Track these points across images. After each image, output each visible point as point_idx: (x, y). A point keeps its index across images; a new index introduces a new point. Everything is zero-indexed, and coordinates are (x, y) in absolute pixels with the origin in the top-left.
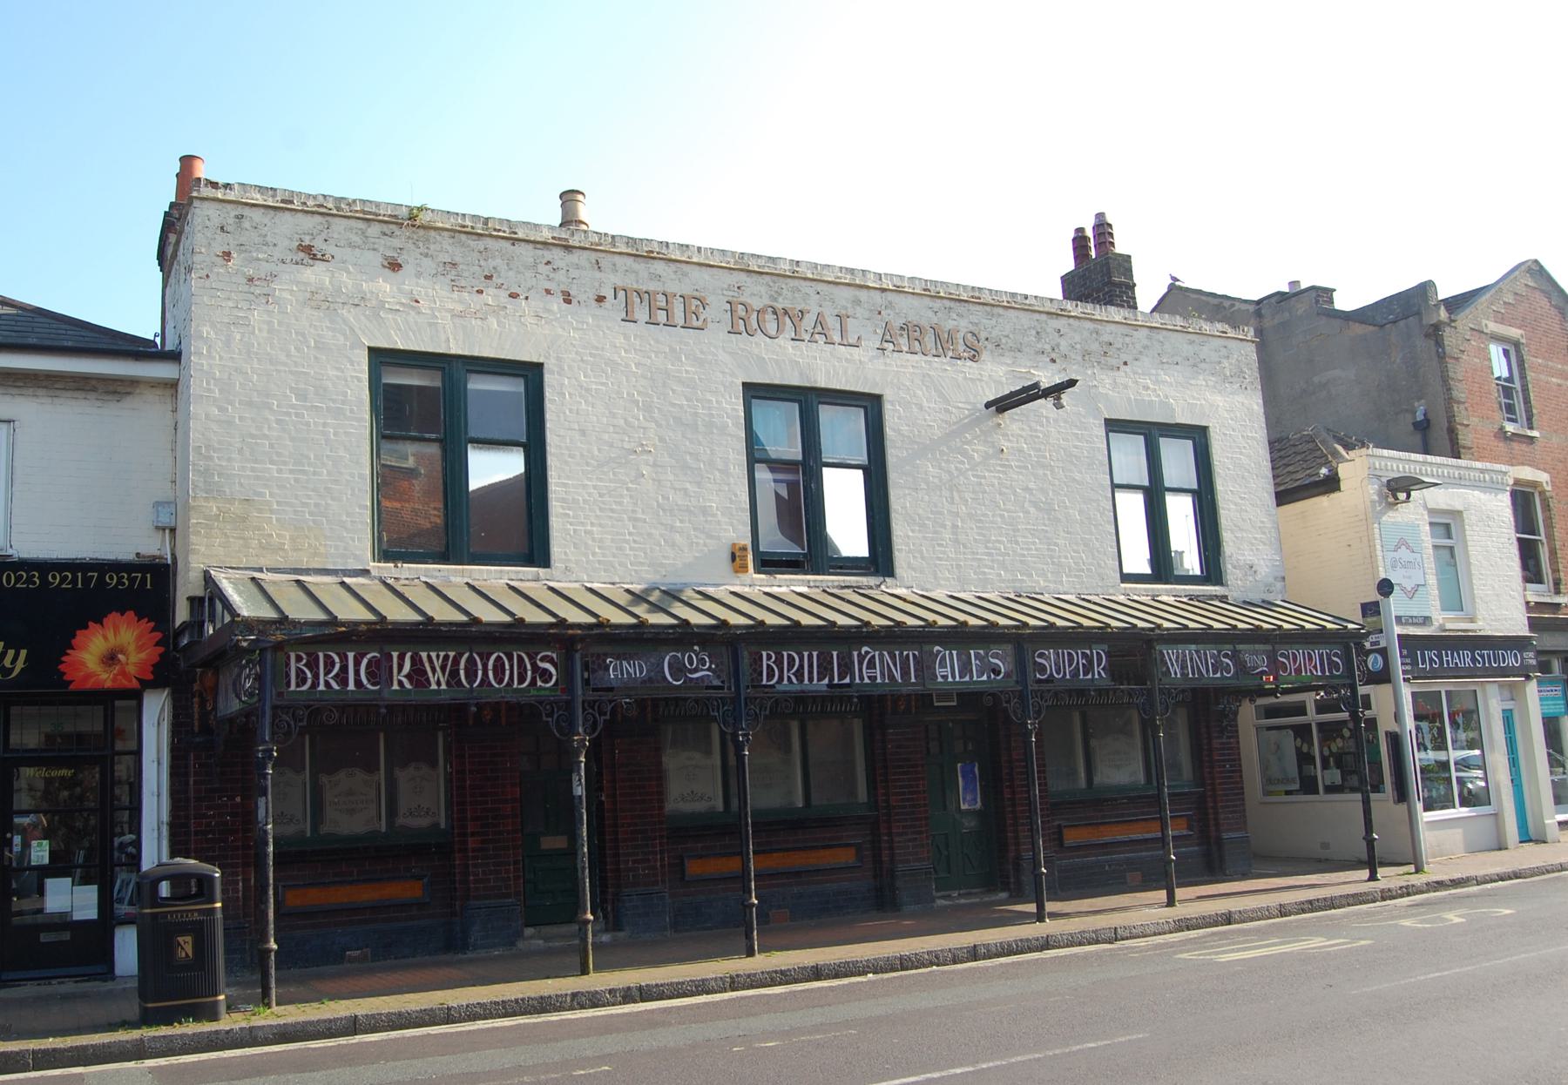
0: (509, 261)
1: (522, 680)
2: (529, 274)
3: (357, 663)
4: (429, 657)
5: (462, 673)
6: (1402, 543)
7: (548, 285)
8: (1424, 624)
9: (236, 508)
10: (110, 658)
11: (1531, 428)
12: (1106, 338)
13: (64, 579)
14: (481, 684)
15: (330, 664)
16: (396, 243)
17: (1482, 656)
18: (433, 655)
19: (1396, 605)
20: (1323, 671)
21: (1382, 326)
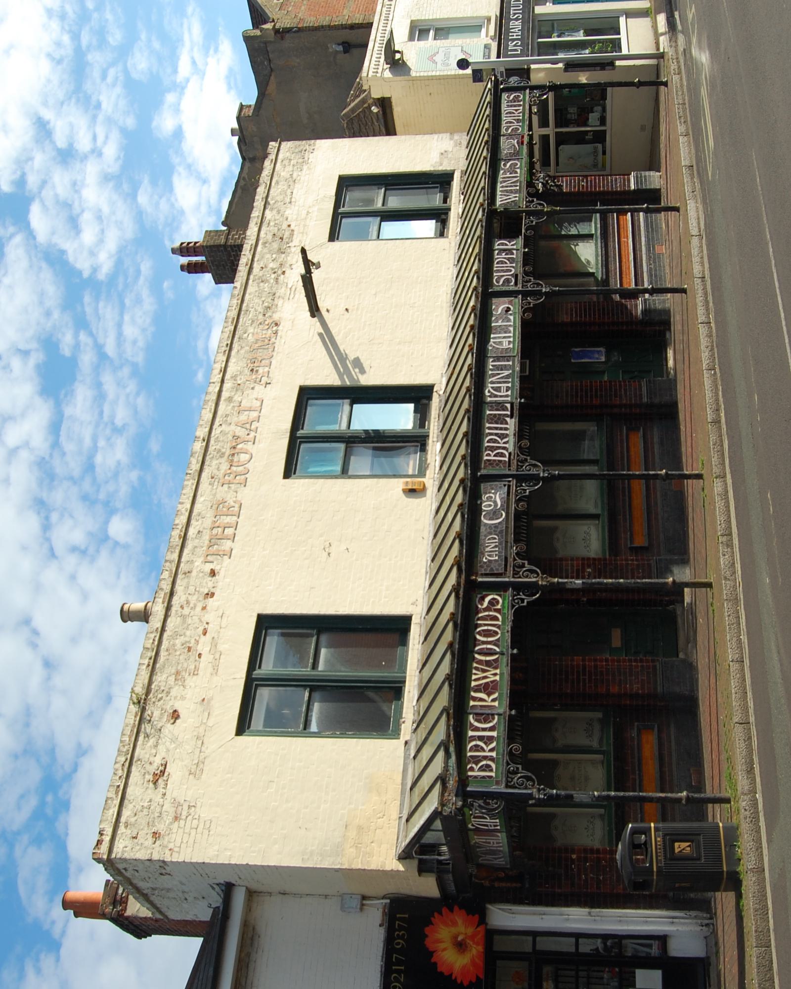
0: (176, 635)
1: (495, 618)
2: (189, 621)
3: (477, 729)
4: (475, 680)
5: (488, 658)
6: (431, 59)
7: (199, 609)
8: (490, 49)
9: (352, 834)
10: (461, 946)
12: (270, 237)
13: (397, 980)
15: (477, 748)
16: (157, 714)
17: (515, 14)
18: (474, 677)
19: (476, 57)
20: (520, 105)
21: (272, 70)
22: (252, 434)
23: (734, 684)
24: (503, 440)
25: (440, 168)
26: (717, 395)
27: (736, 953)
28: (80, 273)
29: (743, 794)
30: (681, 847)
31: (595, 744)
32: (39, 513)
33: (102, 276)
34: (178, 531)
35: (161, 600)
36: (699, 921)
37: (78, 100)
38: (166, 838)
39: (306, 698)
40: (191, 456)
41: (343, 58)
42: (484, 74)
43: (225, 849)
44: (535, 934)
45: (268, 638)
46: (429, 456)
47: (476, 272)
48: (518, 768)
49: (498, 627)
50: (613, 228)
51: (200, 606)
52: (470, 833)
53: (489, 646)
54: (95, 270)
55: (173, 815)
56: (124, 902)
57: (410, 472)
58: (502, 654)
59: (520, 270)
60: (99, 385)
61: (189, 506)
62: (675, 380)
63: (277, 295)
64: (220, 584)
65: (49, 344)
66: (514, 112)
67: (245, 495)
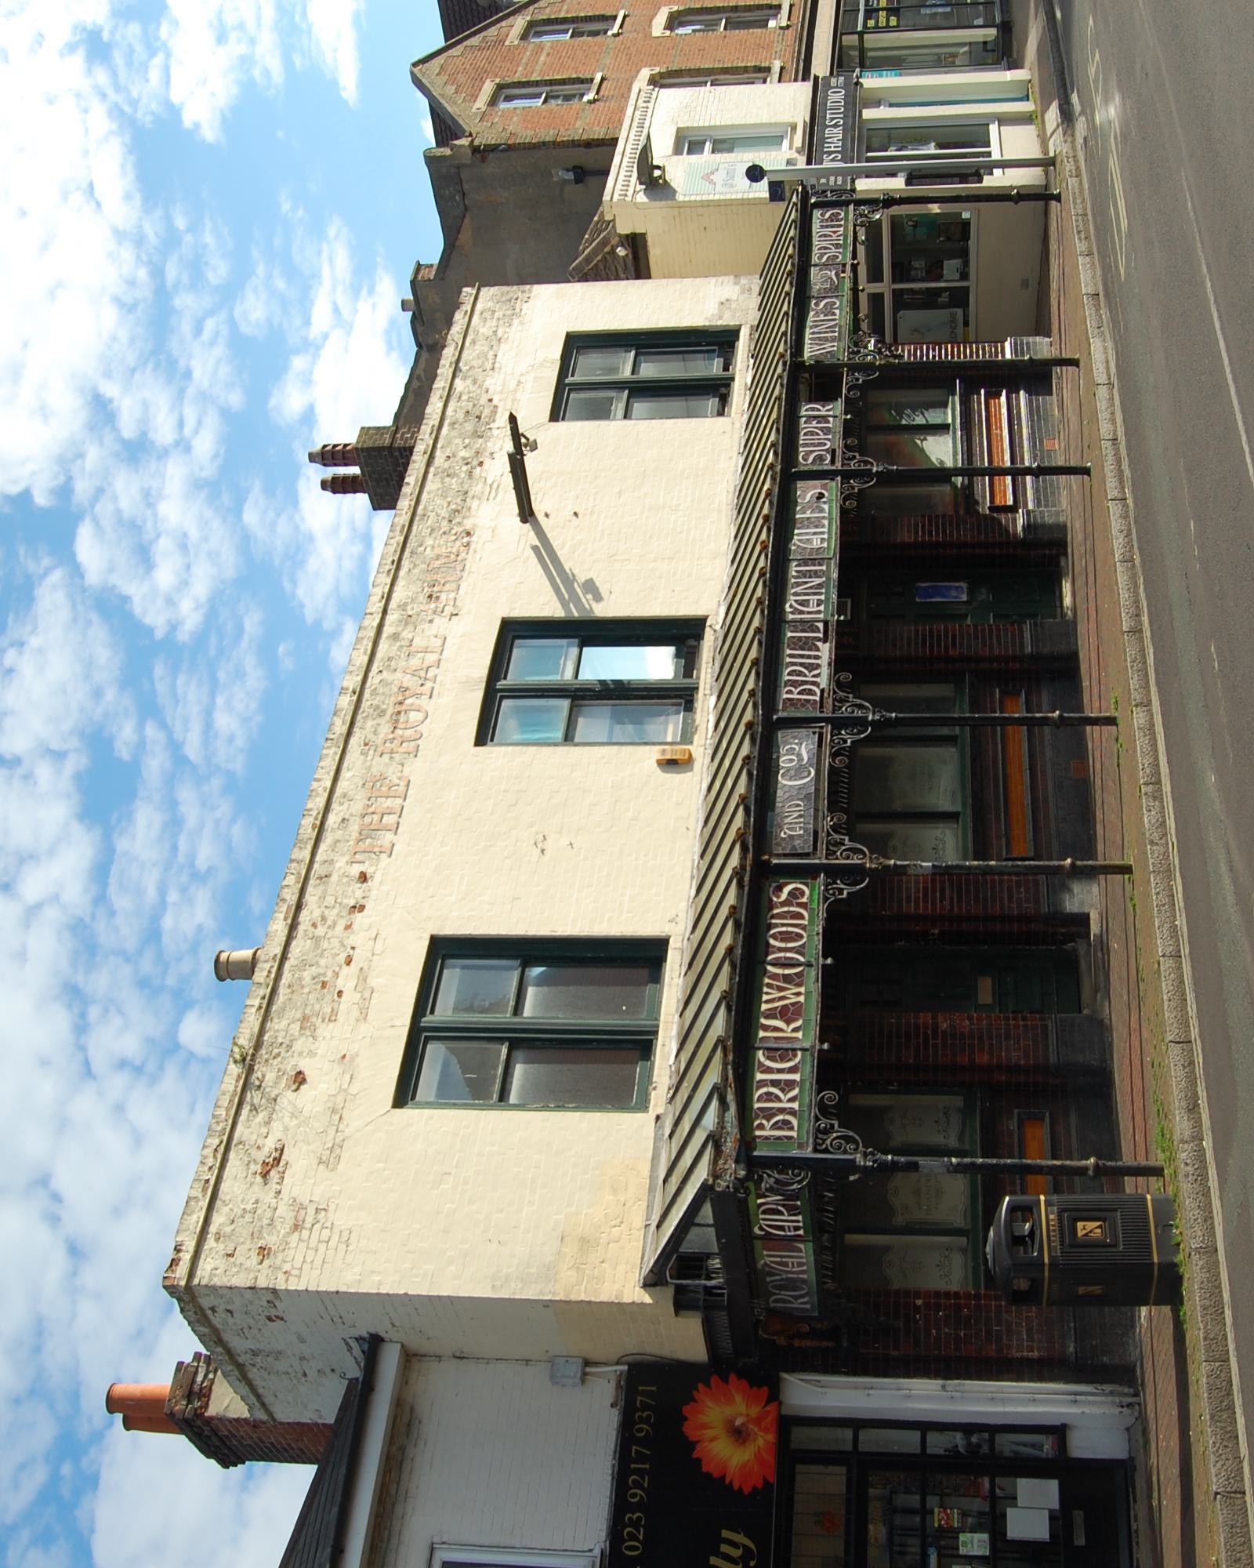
0: (304, 964)
2: (325, 945)
3: (769, 1070)
4: (767, 1002)
5: (787, 972)
6: (708, 178)
7: (340, 927)
9: (570, 1250)
10: (739, 1435)
11: (592, 80)
12: (461, 416)
13: (637, 1484)
14: (803, 955)
15: (769, 1097)
16: (270, 1077)
22: (429, 684)
23: (1166, 986)
24: (812, 671)
25: (719, 323)
26: (1136, 594)
27: (1175, 1412)
28: (150, 631)
29: (1183, 1141)
30: (1083, 1228)
31: (953, 1143)
32: (70, 1007)
33: (183, 636)
34: (312, 819)
35: (282, 916)
36: (1117, 1399)
37: (157, 366)
38: (280, 1256)
39: (503, 1056)
40: (335, 714)
41: (574, 192)
42: (787, 188)
43: (372, 1272)
44: (857, 1424)
45: (445, 971)
46: (698, 716)
47: (773, 445)
48: (832, 1126)
49: (804, 928)
50: (980, 416)
51: (341, 924)
52: (758, 1244)
53: (789, 955)
54: (174, 627)
55: (293, 1221)
56: (205, 1394)
57: (669, 739)
58: (809, 965)
59: (838, 444)
60: (172, 805)
61: (328, 784)
62: (1075, 623)
63: (470, 494)
64: (374, 893)
65: (97, 740)
66: (830, 236)
67: (415, 769)
